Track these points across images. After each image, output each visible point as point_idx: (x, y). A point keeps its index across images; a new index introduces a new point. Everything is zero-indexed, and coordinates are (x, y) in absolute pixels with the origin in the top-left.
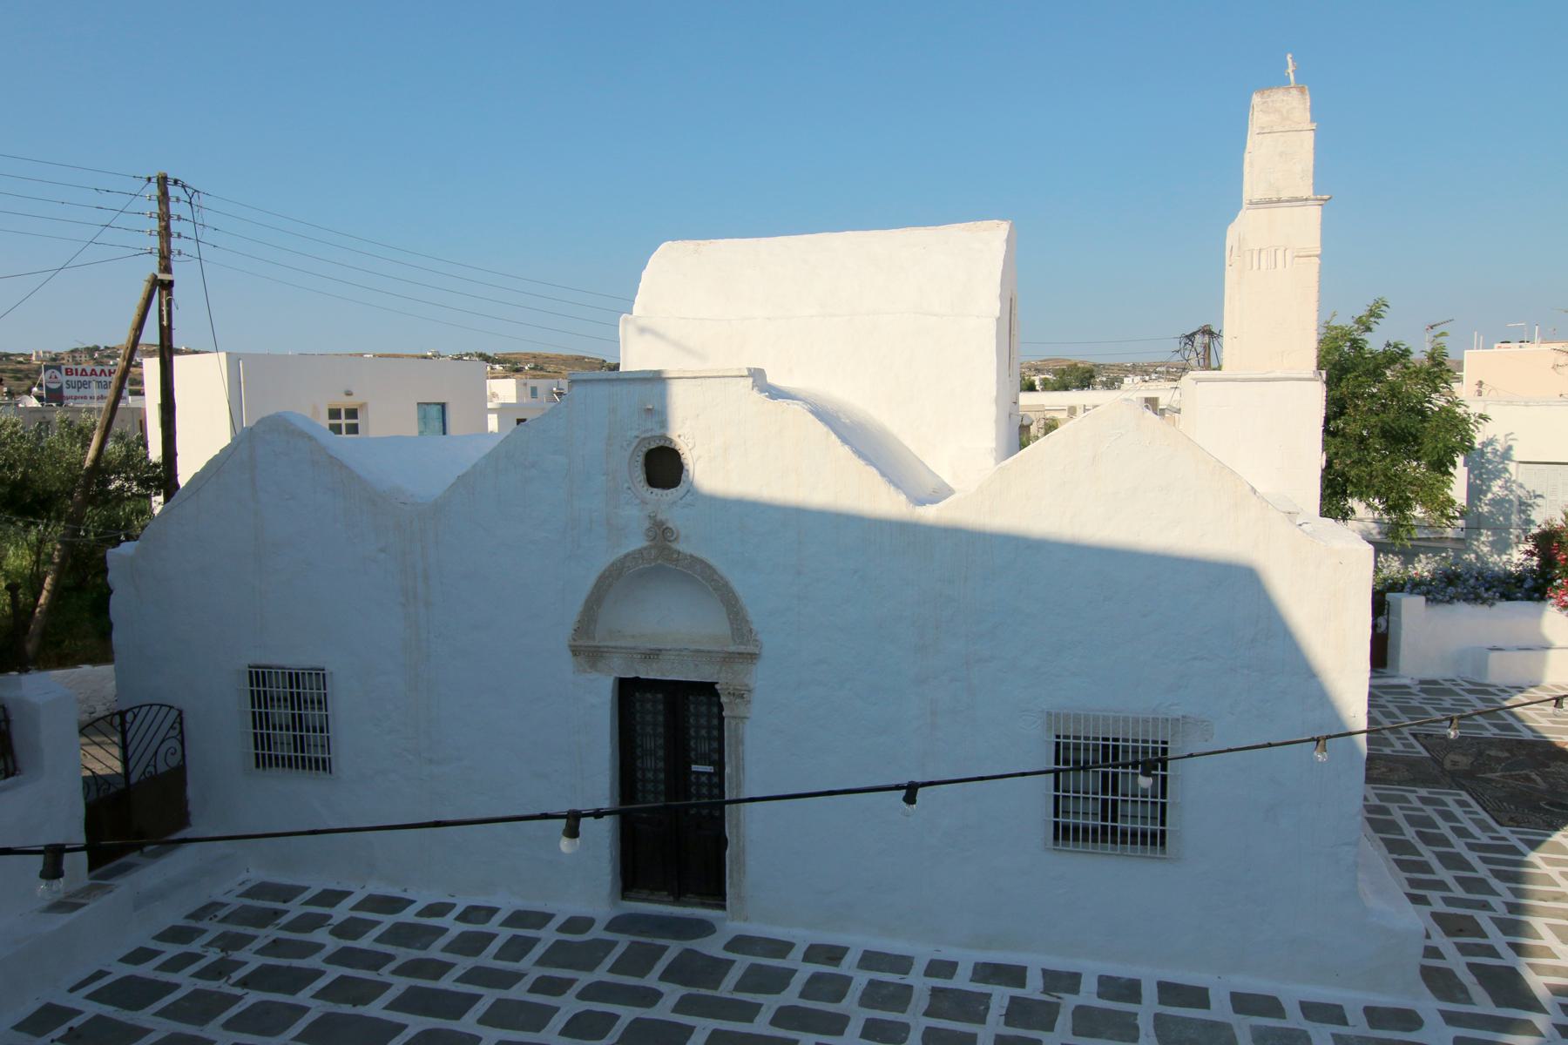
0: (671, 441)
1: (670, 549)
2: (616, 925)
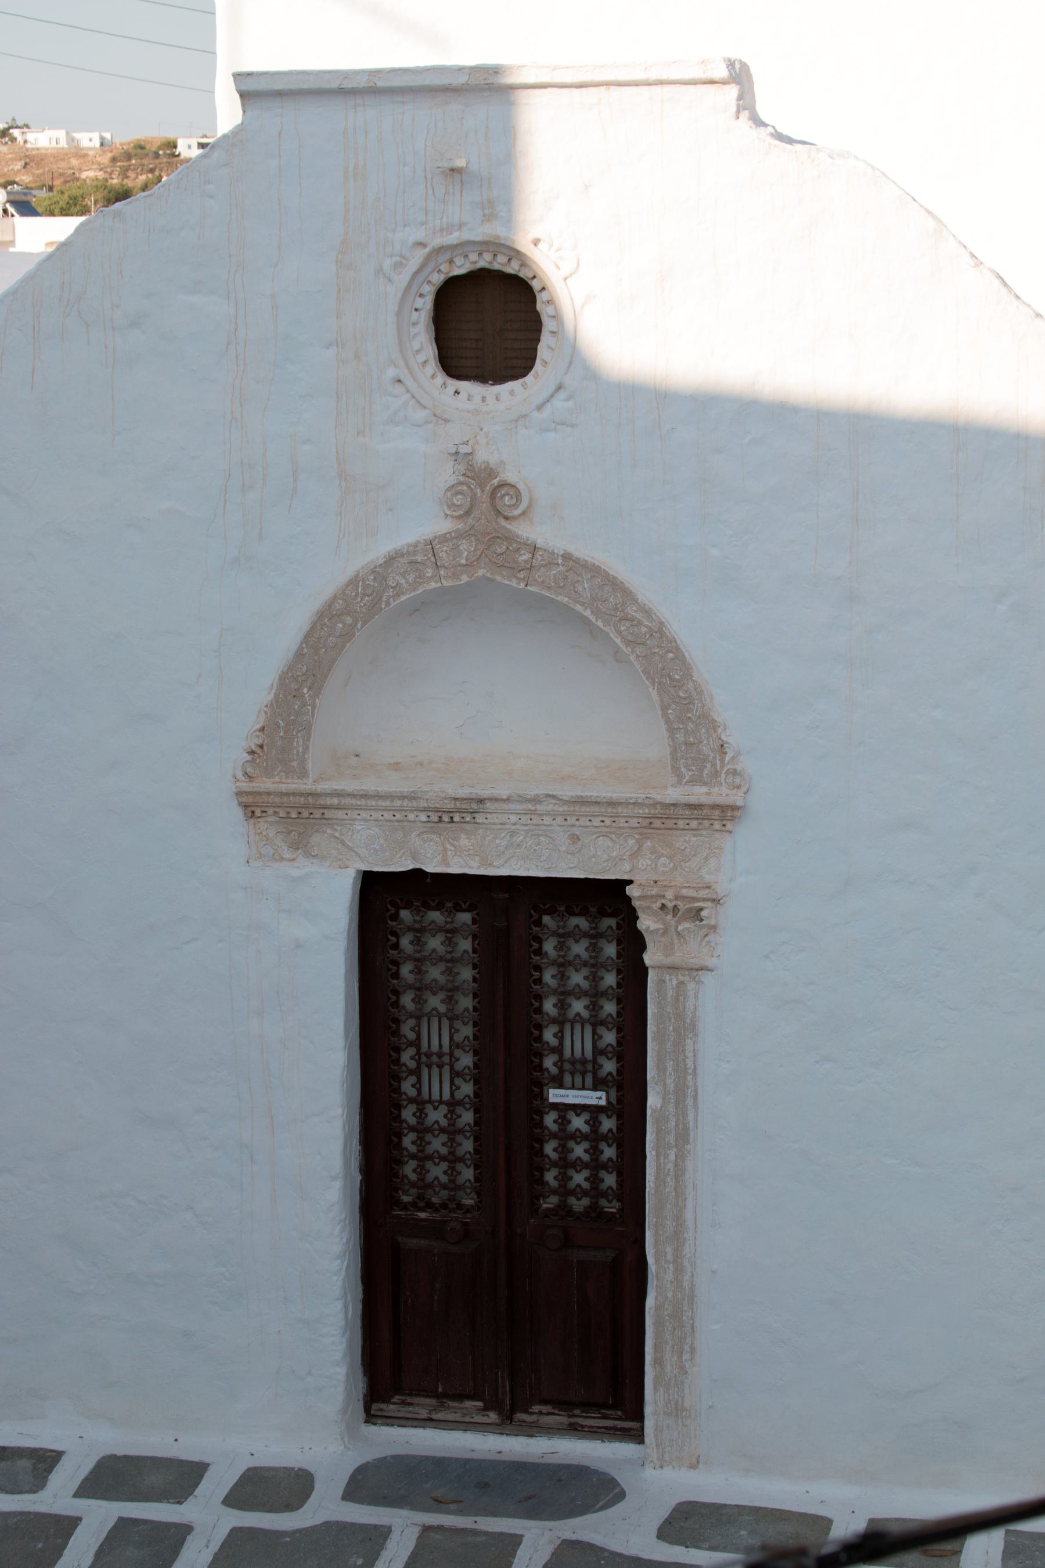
0: (515, 254)
1: (509, 538)
2: (363, 1485)
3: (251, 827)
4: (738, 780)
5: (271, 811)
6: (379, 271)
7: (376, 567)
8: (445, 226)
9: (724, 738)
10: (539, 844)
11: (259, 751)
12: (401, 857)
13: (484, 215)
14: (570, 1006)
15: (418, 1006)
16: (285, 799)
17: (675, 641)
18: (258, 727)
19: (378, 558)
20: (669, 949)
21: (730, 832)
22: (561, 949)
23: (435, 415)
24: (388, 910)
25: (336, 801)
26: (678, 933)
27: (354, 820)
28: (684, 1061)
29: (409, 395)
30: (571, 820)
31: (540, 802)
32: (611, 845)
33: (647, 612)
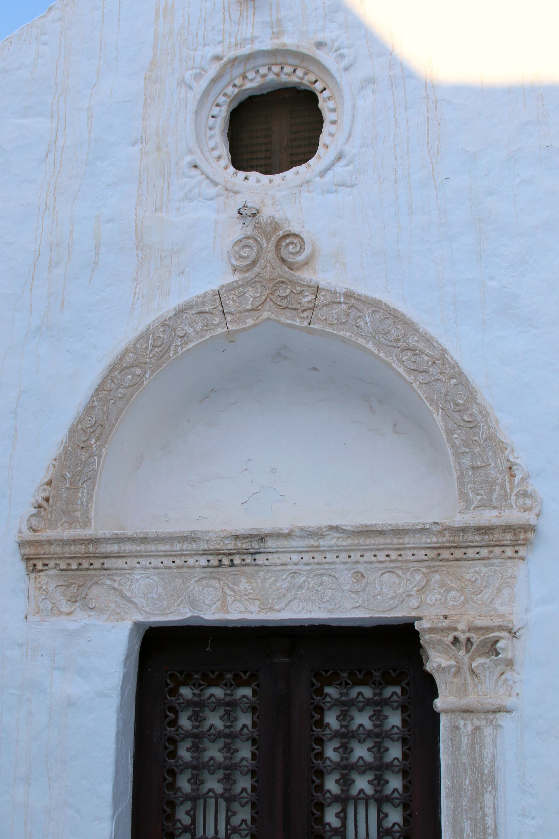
3: (32, 581)
4: (529, 502)
5: (52, 563)
6: (182, 82)
7: (166, 320)
8: (239, 41)
9: (511, 459)
10: (321, 584)
11: (45, 504)
12: (179, 605)
13: (273, 33)
14: (354, 781)
15: (195, 787)
16: (66, 549)
17: (458, 367)
18: (46, 480)
19: (169, 311)
20: (463, 690)
21: (523, 559)
22: (344, 719)
23: (226, 190)
24: (168, 685)
25: (115, 548)
26: (473, 671)
27: (133, 568)
28: (483, 820)
29: (204, 177)
30: (356, 556)
31: (323, 536)
32: (397, 581)
33: (429, 340)
